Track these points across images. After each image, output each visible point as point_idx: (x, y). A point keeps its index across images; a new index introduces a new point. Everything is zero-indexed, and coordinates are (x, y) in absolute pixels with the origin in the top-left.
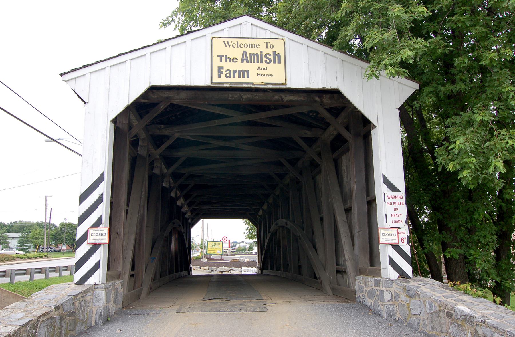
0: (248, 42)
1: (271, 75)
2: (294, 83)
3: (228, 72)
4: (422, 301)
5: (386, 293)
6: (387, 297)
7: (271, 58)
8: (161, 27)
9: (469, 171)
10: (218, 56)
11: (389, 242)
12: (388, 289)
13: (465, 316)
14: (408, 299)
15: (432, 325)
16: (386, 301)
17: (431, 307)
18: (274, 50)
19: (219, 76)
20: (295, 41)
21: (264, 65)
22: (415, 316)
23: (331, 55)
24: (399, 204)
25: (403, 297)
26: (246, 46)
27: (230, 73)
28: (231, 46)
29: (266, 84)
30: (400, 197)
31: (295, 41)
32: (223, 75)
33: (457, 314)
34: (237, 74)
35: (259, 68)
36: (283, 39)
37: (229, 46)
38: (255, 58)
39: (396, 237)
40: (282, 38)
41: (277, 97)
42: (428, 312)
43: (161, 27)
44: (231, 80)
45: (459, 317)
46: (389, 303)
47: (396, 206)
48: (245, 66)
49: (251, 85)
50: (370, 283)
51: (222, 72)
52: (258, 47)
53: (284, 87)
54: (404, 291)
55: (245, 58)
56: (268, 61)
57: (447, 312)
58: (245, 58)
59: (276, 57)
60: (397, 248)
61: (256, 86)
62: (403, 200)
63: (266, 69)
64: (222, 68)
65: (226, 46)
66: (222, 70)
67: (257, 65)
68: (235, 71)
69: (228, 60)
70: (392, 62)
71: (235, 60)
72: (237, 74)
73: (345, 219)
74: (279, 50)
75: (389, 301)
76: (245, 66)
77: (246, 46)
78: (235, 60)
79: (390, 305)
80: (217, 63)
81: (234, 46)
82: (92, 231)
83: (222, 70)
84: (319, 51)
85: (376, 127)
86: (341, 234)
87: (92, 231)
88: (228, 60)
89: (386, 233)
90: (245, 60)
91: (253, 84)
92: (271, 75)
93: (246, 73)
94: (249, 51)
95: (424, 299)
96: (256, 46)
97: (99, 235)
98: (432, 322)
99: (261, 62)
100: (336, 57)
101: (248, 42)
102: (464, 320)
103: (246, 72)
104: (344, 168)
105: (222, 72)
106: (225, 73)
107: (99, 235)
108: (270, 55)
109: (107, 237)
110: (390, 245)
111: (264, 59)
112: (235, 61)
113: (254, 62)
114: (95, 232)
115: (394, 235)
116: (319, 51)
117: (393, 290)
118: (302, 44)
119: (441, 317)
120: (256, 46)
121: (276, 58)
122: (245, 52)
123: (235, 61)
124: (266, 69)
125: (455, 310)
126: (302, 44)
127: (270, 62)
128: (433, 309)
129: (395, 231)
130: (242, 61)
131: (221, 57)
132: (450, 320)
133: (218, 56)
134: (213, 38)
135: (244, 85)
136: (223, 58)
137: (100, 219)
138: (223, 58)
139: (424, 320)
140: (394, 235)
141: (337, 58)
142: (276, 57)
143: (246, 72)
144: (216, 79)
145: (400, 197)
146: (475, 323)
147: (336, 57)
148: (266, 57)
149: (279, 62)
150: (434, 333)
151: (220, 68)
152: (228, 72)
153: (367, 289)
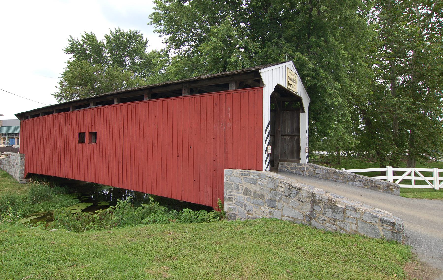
17: (325, 171)
25: (311, 169)
139: (322, 175)
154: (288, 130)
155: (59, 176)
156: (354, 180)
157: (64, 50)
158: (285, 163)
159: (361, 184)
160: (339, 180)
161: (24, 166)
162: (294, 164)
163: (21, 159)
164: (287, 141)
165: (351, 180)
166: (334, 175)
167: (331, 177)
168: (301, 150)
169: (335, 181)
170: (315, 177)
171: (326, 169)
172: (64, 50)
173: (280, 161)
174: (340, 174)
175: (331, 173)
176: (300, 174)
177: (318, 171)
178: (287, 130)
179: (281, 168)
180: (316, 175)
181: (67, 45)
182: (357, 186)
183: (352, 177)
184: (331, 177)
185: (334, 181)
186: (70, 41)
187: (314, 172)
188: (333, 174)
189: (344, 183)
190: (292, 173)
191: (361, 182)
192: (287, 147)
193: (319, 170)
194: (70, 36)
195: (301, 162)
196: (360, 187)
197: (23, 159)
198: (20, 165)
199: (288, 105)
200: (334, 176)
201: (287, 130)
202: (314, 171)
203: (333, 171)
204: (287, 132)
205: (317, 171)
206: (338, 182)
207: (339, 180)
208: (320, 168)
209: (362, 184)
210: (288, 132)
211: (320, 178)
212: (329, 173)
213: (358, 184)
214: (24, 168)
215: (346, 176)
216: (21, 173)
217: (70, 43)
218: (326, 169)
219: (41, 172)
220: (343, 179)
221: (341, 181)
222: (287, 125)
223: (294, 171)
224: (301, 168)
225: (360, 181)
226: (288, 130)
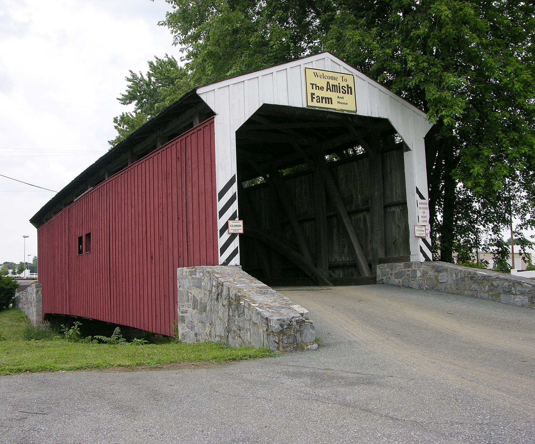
0: (331, 74)
1: (347, 104)
2: (363, 111)
3: (318, 98)
4: (449, 273)
5: (418, 271)
6: (419, 274)
7: (346, 89)
8: (167, 12)
9: (480, 188)
10: (311, 84)
11: (421, 236)
12: (419, 269)
13: (485, 276)
14: (436, 274)
15: (457, 287)
16: (418, 277)
17: (457, 275)
18: (347, 83)
19: (312, 101)
20: (360, 78)
21: (341, 95)
22: (442, 284)
23: (383, 92)
24: (425, 208)
25: (431, 273)
26: (329, 78)
27: (321, 99)
28: (319, 77)
29: (343, 110)
30: (426, 204)
31: (360, 78)
32: (315, 100)
33: (479, 276)
34: (324, 100)
35: (338, 97)
36: (353, 75)
37: (318, 77)
38: (334, 88)
39: (424, 232)
40: (352, 74)
41: (321, 114)
42: (454, 279)
43: (167, 12)
44: (320, 105)
45: (480, 278)
46: (419, 278)
47: (424, 210)
48: (329, 94)
49: (333, 110)
50: (397, 267)
51: (314, 98)
52: (337, 79)
53: (354, 114)
54: (433, 269)
55: (329, 88)
56: (344, 92)
57: (470, 277)
58: (329, 88)
59: (349, 89)
60: (424, 240)
61: (336, 111)
62: (427, 206)
63: (343, 98)
64: (314, 94)
65: (315, 76)
66: (314, 96)
67: (338, 94)
68: (322, 98)
69: (317, 87)
70: (448, 114)
71: (322, 88)
72: (324, 100)
73: (349, 221)
74: (351, 85)
75: (419, 277)
76: (329, 94)
77: (329, 78)
78: (322, 88)
79: (420, 280)
80: (310, 91)
81: (321, 77)
82: (231, 223)
83: (314, 96)
84: (376, 87)
85: (410, 150)
86: (350, 234)
87: (231, 223)
88: (317, 87)
89: (419, 229)
90: (329, 89)
91: (335, 109)
92: (347, 104)
93: (329, 100)
94: (332, 82)
95: (451, 271)
96: (335, 79)
97: (237, 226)
98: (457, 285)
99: (340, 92)
100: (386, 94)
101: (331, 74)
102: (483, 279)
103: (330, 100)
104: (341, 177)
105: (314, 98)
106: (316, 99)
107: (237, 226)
108: (345, 87)
109: (242, 228)
110: (421, 238)
111: (341, 90)
112: (322, 89)
113: (335, 92)
114: (234, 224)
115: (423, 231)
116: (376, 87)
117: (422, 269)
118: (365, 81)
119: (465, 281)
120: (335, 79)
121: (349, 90)
122: (328, 83)
123: (322, 89)
124: (343, 98)
125: (476, 275)
126: (365, 81)
127: (345, 93)
128: (459, 277)
129: (424, 228)
130: (327, 91)
131: (312, 84)
132: (473, 281)
133: (311, 84)
134: (306, 68)
135: (329, 110)
136: (314, 86)
137: (235, 213)
138: (314, 86)
139: (451, 285)
140: (423, 231)
141: (387, 94)
142: (349, 89)
143: (330, 100)
144: (310, 104)
145: (426, 204)
146: (491, 280)
147: (386, 94)
148: (342, 89)
149: (351, 94)
150: (459, 291)
151: (313, 94)
152: (318, 98)
153: (393, 272)
154: (396, 193)
155: (97, 319)
156: (510, 292)
157: (119, 99)
158: (386, 265)
159: (525, 300)
160: (482, 294)
161: (41, 303)
162: (400, 266)
163: (37, 292)
164: (397, 217)
165: (505, 292)
166: (474, 283)
167: (467, 288)
168: (410, 233)
169: (474, 296)
170: (439, 291)
171: (457, 271)
172: (119, 99)
173: (381, 261)
174: (483, 279)
175: (466, 279)
176: (409, 287)
177: (443, 277)
178: (394, 193)
179: (381, 278)
180: (440, 286)
181: (124, 88)
182: (518, 304)
183: (506, 284)
184: (467, 288)
185: (472, 296)
186: (129, 80)
187: (436, 279)
188: (470, 281)
189: (492, 300)
190: (398, 286)
191: (524, 296)
192: (397, 231)
193: (444, 273)
194: (131, 71)
195: (413, 259)
196: (523, 306)
197: (40, 292)
198: (36, 301)
199: (285, 168)
200: (473, 286)
201: (394, 193)
202: (436, 277)
203: (470, 273)
204: (395, 198)
205: (442, 276)
206: (482, 298)
207: (482, 294)
208: (446, 270)
209: (527, 300)
210: (396, 196)
211: (448, 292)
212: (463, 279)
213: (519, 299)
214: (41, 306)
215: (495, 283)
216: (38, 315)
217: (130, 83)
218: (457, 271)
219: (83, 314)
220: (490, 290)
221: (486, 295)
222: (394, 181)
223: (400, 282)
224: (410, 272)
225: (522, 293)
226: (396, 193)
